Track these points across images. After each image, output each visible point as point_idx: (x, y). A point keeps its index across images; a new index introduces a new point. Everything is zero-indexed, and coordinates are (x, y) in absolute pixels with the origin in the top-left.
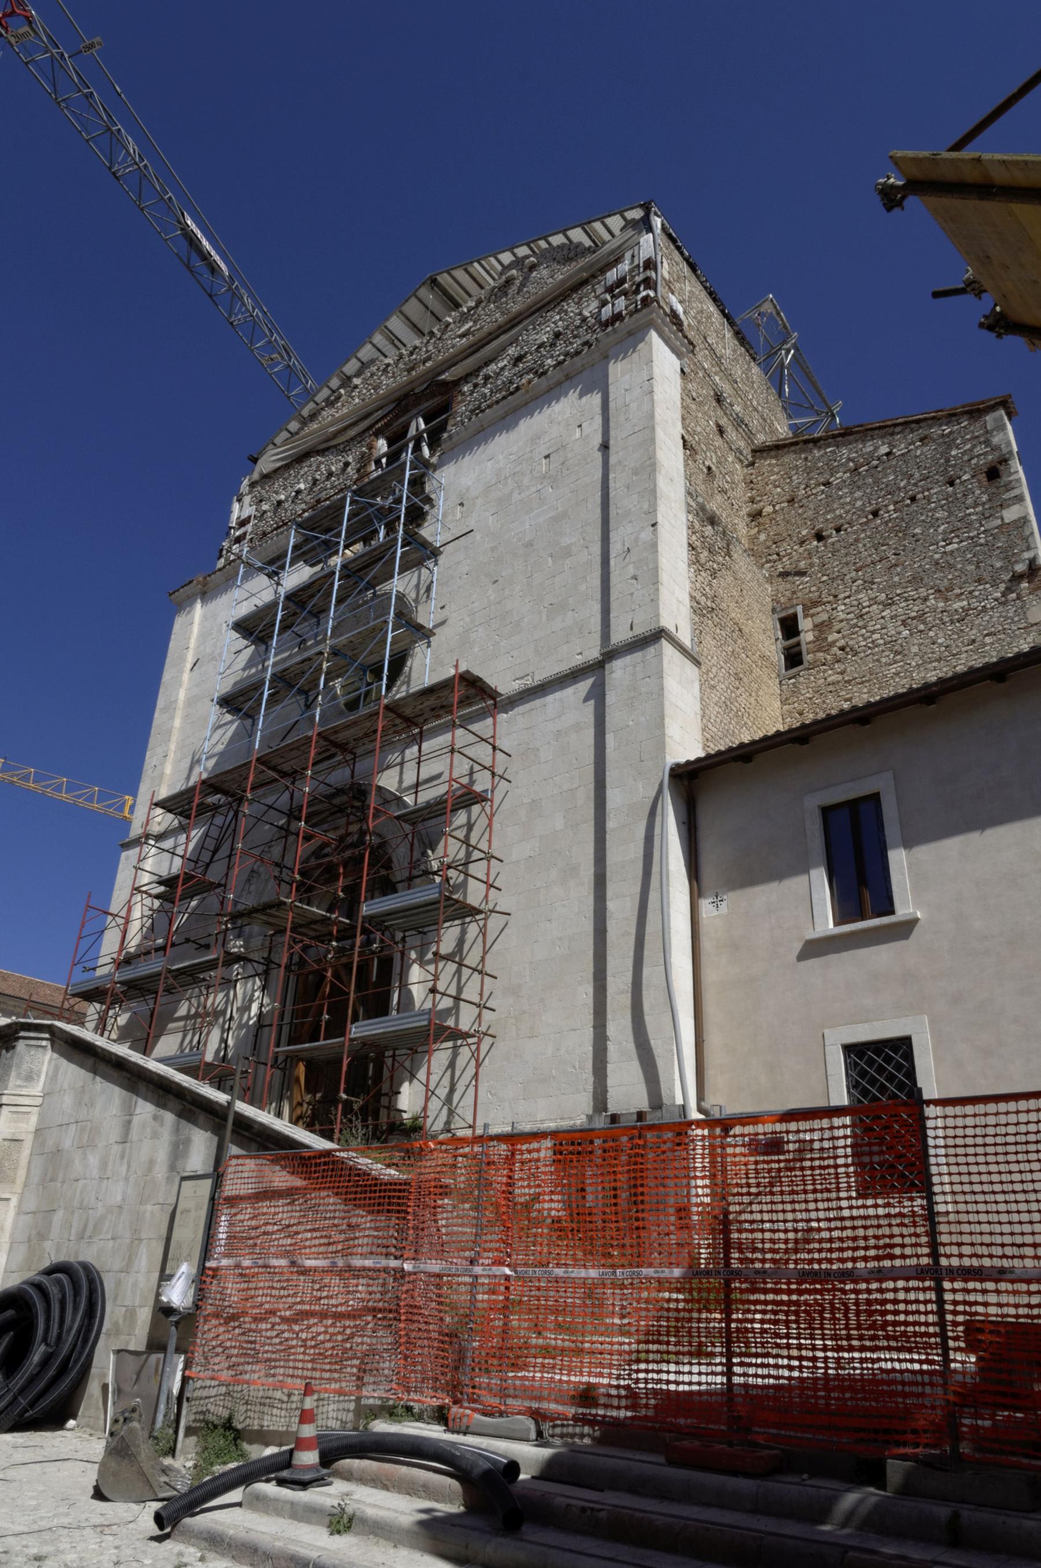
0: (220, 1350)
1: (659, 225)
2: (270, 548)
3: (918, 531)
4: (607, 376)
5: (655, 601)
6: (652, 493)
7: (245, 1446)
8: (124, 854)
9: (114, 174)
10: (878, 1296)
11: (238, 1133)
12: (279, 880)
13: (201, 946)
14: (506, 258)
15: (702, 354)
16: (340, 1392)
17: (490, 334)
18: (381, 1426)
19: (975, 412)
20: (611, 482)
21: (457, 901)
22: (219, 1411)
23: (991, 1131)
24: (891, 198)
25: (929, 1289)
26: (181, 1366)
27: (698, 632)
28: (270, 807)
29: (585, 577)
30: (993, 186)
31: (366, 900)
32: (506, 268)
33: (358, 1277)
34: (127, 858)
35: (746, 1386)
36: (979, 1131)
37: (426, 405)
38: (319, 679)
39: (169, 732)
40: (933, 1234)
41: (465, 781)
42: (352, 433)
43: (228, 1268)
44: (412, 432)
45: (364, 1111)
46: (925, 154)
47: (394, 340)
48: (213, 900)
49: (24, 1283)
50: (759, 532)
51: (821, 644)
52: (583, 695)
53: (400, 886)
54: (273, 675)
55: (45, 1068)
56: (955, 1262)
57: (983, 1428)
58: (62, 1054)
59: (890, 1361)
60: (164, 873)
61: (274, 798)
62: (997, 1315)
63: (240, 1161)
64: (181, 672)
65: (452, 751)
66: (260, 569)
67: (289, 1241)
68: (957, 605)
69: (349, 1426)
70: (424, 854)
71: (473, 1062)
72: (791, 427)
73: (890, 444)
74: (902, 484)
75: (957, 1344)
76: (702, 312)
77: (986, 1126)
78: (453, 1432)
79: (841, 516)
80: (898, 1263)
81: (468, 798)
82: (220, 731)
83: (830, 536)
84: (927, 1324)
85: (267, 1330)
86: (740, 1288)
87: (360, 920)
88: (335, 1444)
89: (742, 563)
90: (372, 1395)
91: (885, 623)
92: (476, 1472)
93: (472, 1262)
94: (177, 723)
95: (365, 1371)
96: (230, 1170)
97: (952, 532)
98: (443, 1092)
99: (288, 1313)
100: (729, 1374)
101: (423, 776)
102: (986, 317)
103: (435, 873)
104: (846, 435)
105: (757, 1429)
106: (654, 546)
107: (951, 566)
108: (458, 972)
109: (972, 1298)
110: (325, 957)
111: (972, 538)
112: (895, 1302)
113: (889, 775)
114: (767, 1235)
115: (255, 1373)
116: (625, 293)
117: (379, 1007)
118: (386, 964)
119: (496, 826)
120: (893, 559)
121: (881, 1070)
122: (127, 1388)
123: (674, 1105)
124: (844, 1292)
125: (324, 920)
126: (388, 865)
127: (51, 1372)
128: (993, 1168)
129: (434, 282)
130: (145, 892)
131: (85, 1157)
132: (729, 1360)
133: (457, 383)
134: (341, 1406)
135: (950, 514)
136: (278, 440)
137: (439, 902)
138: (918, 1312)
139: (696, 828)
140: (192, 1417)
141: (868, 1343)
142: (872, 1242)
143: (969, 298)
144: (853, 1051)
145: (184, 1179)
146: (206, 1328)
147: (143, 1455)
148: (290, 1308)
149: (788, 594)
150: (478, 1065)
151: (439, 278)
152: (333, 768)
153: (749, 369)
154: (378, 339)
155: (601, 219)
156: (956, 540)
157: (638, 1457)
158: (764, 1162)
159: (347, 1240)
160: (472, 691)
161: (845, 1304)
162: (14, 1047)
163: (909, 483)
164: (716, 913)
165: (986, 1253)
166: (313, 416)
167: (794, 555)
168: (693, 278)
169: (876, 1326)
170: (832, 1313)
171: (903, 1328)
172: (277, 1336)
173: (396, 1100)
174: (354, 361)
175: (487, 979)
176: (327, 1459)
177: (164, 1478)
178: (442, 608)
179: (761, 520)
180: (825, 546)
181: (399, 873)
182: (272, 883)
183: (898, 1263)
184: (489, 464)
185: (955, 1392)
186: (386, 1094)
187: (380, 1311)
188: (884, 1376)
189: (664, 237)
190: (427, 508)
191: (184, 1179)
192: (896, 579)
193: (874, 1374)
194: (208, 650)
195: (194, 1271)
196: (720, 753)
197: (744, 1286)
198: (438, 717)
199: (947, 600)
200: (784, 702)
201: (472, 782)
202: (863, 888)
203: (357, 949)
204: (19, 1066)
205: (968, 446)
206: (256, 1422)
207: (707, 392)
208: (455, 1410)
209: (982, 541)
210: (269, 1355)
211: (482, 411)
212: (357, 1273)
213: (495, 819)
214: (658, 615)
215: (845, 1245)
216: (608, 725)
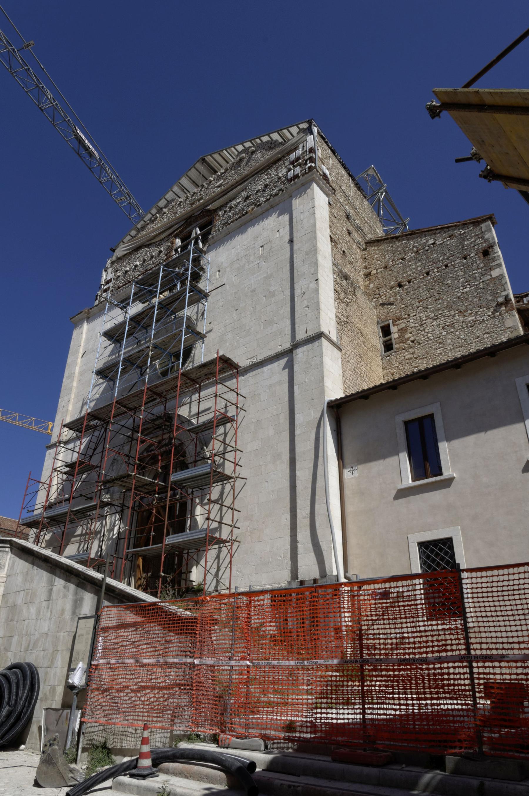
0: (99, 707)
2: (122, 294)
3: (449, 282)
5: (318, 318)
6: (315, 264)
7: (113, 757)
8: (48, 452)
9: (40, 108)
10: (440, 671)
11: (108, 594)
12: (128, 464)
13: (88, 498)
14: (240, 148)
15: (339, 195)
16: (162, 728)
17: (232, 186)
18: (184, 745)
21: (220, 473)
22: (99, 739)
24: (434, 112)
25: (466, 667)
26: (79, 716)
27: (340, 334)
28: (123, 426)
29: (282, 307)
30: (485, 105)
31: (173, 473)
32: (240, 153)
35: (372, 719)
36: (489, 585)
39: (71, 389)
40: (467, 638)
41: (223, 411)
42: (163, 236)
43: (103, 664)
44: (193, 235)
47: (184, 189)
48: (94, 474)
50: (370, 283)
51: (402, 339)
53: (190, 465)
54: (124, 359)
55: (7, 563)
56: (478, 652)
59: (447, 704)
60: (69, 461)
61: (125, 421)
62: (500, 679)
63: (109, 609)
64: (77, 358)
65: (216, 396)
67: (135, 650)
69: (167, 745)
70: (202, 449)
71: (229, 555)
72: (384, 231)
73: (434, 239)
74: (441, 259)
75: (480, 695)
76: (338, 174)
77: (493, 582)
78: (221, 747)
80: (449, 654)
82: (97, 388)
83: (405, 285)
84: (465, 685)
85: (124, 696)
89: (361, 299)
90: (179, 729)
91: (434, 328)
92: (234, 768)
94: (75, 384)
95: (175, 717)
96: (104, 613)
97: (466, 282)
98: (213, 571)
99: (135, 687)
100: (364, 713)
101: (201, 409)
102: (483, 172)
103: (208, 459)
104: (412, 234)
105: (379, 742)
106: (317, 291)
107: (466, 299)
108: (221, 509)
109: (487, 671)
112: (448, 674)
113: (438, 404)
114: (382, 641)
115: (118, 719)
116: (300, 165)
117: (180, 528)
118: (184, 506)
119: (239, 434)
121: (437, 555)
122: (52, 727)
123: (332, 575)
124: (422, 669)
125: (151, 484)
126: (184, 455)
127: (12, 720)
128: (497, 604)
129: (203, 160)
130: (59, 471)
132: (363, 706)
133: (216, 210)
134: (163, 735)
135: (465, 273)
136: (125, 240)
137: (210, 473)
138: (460, 679)
139: (341, 433)
140: (85, 743)
141: (435, 696)
142: (436, 643)
145: (80, 618)
146: (92, 696)
148: (136, 685)
149: (385, 314)
150: (231, 557)
152: (155, 406)
153: (363, 202)
154: (176, 189)
155: (287, 128)
156: (468, 286)
157: (317, 758)
158: (379, 603)
159: (165, 648)
160: (226, 365)
163: (444, 258)
164: (352, 476)
165: (494, 647)
166: (143, 228)
167: (387, 295)
168: (334, 157)
169: (439, 687)
171: (452, 687)
172: (129, 699)
174: (163, 200)
175: (235, 512)
176: (156, 763)
177: (72, 775)
178: (210, 323)
180: (403, 290)
181: (190, 459)
182: (124, 465)
183: (449, 654)
184: (233, 251)
185: (480, 720)
186: (184, 573)
187: (182, 685)
188: (444, 712)
189: (319, 137)
190: (201, 273)
191: (80, 618)
192: (439, 306)
193: (438, 712)
195: (86, 666)
196: (352, 395)
198: (209, 379)
199: (464, 316)
200: (384, 369)
201: (226, 411)
202: (426, 463)
205: (473, 240)
206: (119, 744)
208: (222, 736)
209: (481, 287)
210: (125, 709)
213: (238, 430)
215: (422, 645)
216: (295, 381)
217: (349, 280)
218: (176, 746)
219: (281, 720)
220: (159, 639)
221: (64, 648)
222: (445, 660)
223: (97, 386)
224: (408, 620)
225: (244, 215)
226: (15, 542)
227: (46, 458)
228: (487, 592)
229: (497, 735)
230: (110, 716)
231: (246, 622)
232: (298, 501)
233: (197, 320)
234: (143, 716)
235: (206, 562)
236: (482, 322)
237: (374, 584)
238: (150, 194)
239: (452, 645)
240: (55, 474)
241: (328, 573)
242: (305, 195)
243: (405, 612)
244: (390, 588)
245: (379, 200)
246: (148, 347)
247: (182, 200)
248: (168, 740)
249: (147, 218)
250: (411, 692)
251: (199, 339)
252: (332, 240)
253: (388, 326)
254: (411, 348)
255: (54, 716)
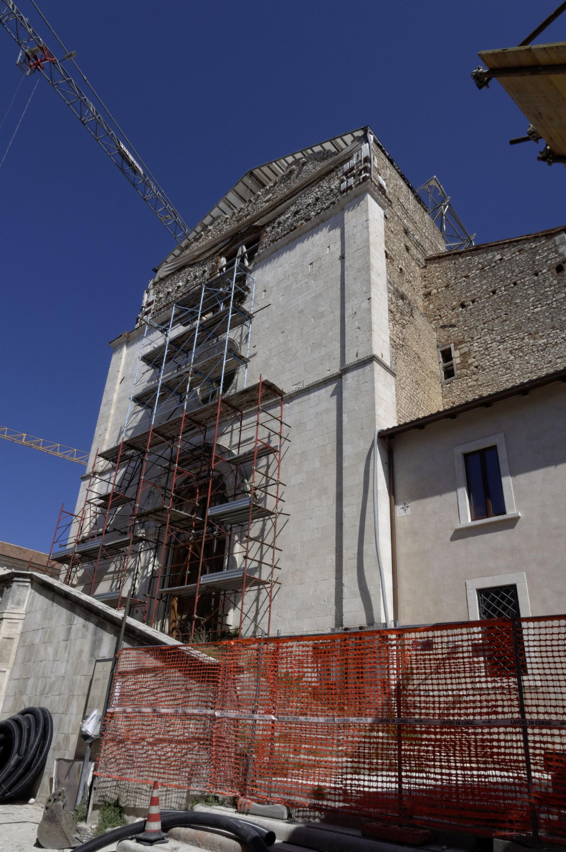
0: (113, 760)
1: (372, 139)
2: (162, 317)
3: (518, 301)
4: (343, 219)
5: (370, 340)
6: (368, 282)
7: (126, 817)
8: (83, 483)
9: (83, 122)
10: (488, 737)
11: (128, 636)
12: (165, 497)
13: (122, 533)
14: (290, 159)
15: (396, 208)
16: (178, 787)
17: (281, 200)
18: (200, 808)
19: (549, 235)
20: (346, 276)
21: (260, 507)
22: (112, 796)
23: (555, 637)
24: (481, 81)
25: (519, 733)
26: (92, 769)
27: (394, 358)
28: (160, 456)
29: (331, 328)
30: (540, 66)
31: (210, 507)
32: (290, 165)
33: (190, 719)
34: (84, 485)
35: (409, 790)
36: (548, 637)
37: (247, 239)
38: (186, 386)
39: (108, 417)
40: (521, 699)
41: (265, 441)
42: (207, 255)
43: (119, 713)
44: (239, 253)
45: (208, 625)
46: (499, 50)
47: (230, 205)
48: (128, 507)
49: (9, 719)
50: (429, 304)
51: (465, 364)
52: (330, 393)
53: (230, 499)
54: (162, 384)
55: (27, 598)
56: (535, 717)
57: (553, 821)
58: (37, 591)
59: (496, 775)
60: (103, 492)
61: (163, 451)
62: (560, 750)
63: (128, 652)
64: (115, 384)
65: (258, 424)
66: (157, 328)
67: (153, 698)
68: (541, 342)
69: (183, 807)
70: (243, 481)
71: (268, 598)
72: (447, 247)
73: (502, 254)
74: (509, 276)
75: (536, 767)
76: (396, 185)
77: (552, 634)
78: (240, 813)
79: (475, 294)
80: (500, 717)
81: (267, 450)
82: (135, 416)
83: (469, 305)
84: (517, 755)
85: (139, 749)
86: (406, 730)
87: (206, 518)
88: (171, 818)
89: (420, 321)
90: (196, 789)
91: (500, 353)
92: (249, 838)
93: (253, 712)
94: (112, 411)
95: (192, 775)
96: (122, 656)
97: (537, 301)
98: (252, 615)
99: (151, 740)
100: (400, 782)
101: (243, 439)
102: (541, 153)
103: (248, 492)
104: (478, 249)
105: (416, 817)
106: (369, 310)
107: (537, 320)
108: (261, 547)
109: (545, 739)
110: (188, 539)
111: (549, 304)
112: (499, 741)
113: (502, 435)
114: (423, 699)
115: (132, 775)
116: (354, 176)
117: (218, 567)
118: (222, 544)
119: (282, 466)
120: (504, 317)
121: (499, 604)
122: (62, 781)
123: (380, 623)
124: (468, 734)
125: (188, 518)
126: (223, 487)
127: (21, 771)
128: (557, 660)
129: (252, 174)
130: (93, 503)
131: (46, 649)
132: (400, 774)
133: (263, 227)
134: (179, 795)
135: (536, 291)
136: (168, 260)
137: (249, 508)
138: (512, 747)
139: (393, 466)
140: (98, 799)
141: (482, 766)
142: (485, 704)
143: (532, 143)
144: (482, 593)
145: (98, 661)
146: (107, 747)
147: (64, 821)
148: (152, 737)
149: (446, 337)
150: (271, 601)
151: (254, 172)
152: (192, 435)
153: (423, 216)
154: (222, 205)
155: (341, 137)
156: (539, 306)
157: (346, 831)
158: (421, 655)
159: (185, 697)
160: (269, 391)
161: (468, 742)
162: (11, 586)
163: (512, 275)
164: (404, 514)
165: (553, 712)
166: (187, 247)
167: (449, 316)
168: (392, 167)
169: (487, 755)
170: (461, 747)
171: (503, 757)
172: (145, 753)
173: (226, 619)
174: (209, 217)
175: (276, 551)
176: (166, 827)
177: (78, 836)
178: (254, 347)
179: (430, 297)
180: (466, 311)
181: (230, 493)
182: (161, 499)
183: (500, 717)
184: (280, 269)
185: (535, 797)
186: (220, 616)
187: (201, 739)
188: (492, 786)
189: (375, 145)
190: (246, 293)
191: (98, 661)
192: (506, 328)
193: (485, 785)
194: (129, 372)
195: (101, 714)
196: (406, 424)
197: (409, 729)
198: (251, 406)
199: (535, 339)
200: (444, 397)
201: (270, 441)
202: (487, 500)
203: (205, 535)
204: (13, 597)
205: (546, 254)
206: (132, 803)
207: (400, 228)
208: (242, 800)
209: (554, 306)
210: (140, 764)
211: (277, 240)
212: (190, 717)
213: (282, 462)
214: (371, 348)
215: (469, 705)
216: (344, 409)
217: (406, 299)
218: (192, 808)
219: (306, 785)
220: (179, 687)
221: (80, 693)
222: (495, 724)
223: (135, 413)
224: (453, 675)
225: (292, 231)
226: (36, 577)
227: (81, 489)
228: (546, 646)
229: (556, 817)
230: (124, 771)
231: (272, 671)
232: (344, 540)
233: (240, 343)
234: (158, 773)
235: (243, 604)
236: (555, 345)
237: (415, 632)
238: (196, 209)
239: (503, 706)
240: (88, 506)
241: (376, 621)
242: (359, 208)
243: (450, 666)
244: (434, 637)
245: (442, 214)
246: (188, 372)
247: (228, 216)
248: (184, 801)
249: (191, 237)
250: (455, 760)
251: (242, 364)
252: (387, 256)
253: (449, 350)
254: (474, 374)
255: (66, 766)
